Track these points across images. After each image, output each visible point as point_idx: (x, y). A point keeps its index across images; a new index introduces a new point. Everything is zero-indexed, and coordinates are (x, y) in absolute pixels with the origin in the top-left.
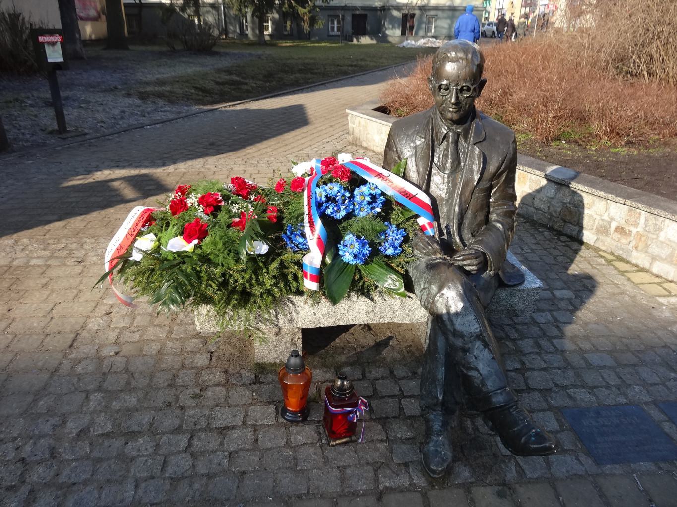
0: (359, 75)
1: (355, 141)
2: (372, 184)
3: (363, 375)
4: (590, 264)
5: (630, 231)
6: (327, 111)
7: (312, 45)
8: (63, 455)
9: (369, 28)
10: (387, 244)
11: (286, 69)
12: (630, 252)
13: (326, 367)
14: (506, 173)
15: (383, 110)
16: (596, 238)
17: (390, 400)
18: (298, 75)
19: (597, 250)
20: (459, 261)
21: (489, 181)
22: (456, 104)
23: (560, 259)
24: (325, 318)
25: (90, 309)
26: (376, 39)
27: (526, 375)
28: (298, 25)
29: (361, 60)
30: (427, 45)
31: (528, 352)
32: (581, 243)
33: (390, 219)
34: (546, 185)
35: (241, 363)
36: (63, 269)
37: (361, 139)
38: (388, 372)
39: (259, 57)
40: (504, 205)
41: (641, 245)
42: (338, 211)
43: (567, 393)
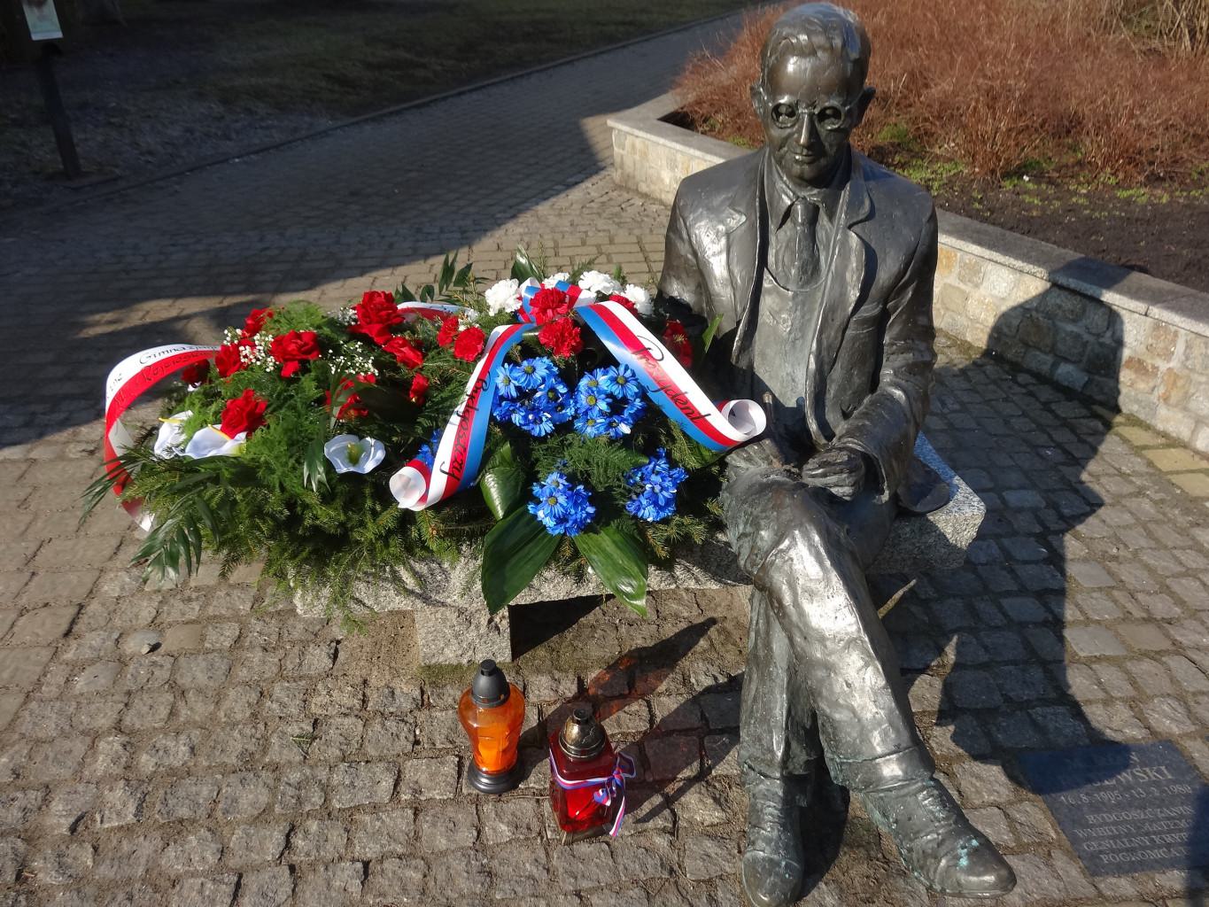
0: (638, 42)
1: (626, 182)
5: (1154, 367)
8: (41, 876)
12: (1153, 409)
16: (1086, 379)
17: (682, 740)
20: (813, 476)
22: (809, 146)
24: (551, 586)
25: (108, 552)
35: (393, 664)
36: (60, 467)
41: (1175, 396)
42: (538, 420)
43: (1029, 715)
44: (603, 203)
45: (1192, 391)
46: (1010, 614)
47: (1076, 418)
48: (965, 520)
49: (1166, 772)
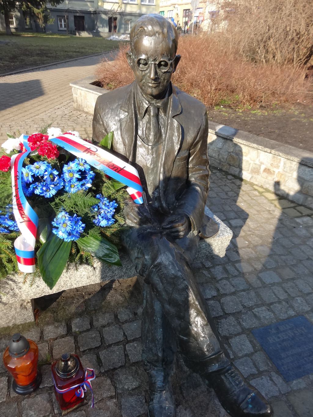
0: (81, 59)
2: (80, 160)
3: (91, 324)
4: (250, 196)
5: (274, 172)
6: (58, 85)
7: (47, 36)
9: (86, 26)
10: (100, 217)
11: (27, 53)
13: (57, 321)
14: (201, 142)
15: (98, 84)
16: (251, 176)
17: (116, 348)
18: (36, 58)
19: (252, 184)
21: (187, 150)
23: (230, 194)
26: (92, 34)
27: (221, 301)
28: (35, 21)
29: (82, 48)
30: (126, 40)
31: (219, 278)
32: (241, 180)
33: (101, 191)
34: (216, 140)
37: (83, 106)
38: (113, 317)
39: (7, 44)
40: (200, 170)
42: (48, 189)
43: (253, 312)
44: (70, 116)
45: (286, 179)
46: (239, 270)
47: (249, 191)
48: (226, 238)
49: (304, 329)
